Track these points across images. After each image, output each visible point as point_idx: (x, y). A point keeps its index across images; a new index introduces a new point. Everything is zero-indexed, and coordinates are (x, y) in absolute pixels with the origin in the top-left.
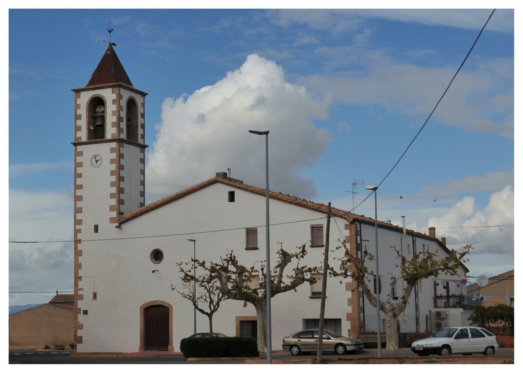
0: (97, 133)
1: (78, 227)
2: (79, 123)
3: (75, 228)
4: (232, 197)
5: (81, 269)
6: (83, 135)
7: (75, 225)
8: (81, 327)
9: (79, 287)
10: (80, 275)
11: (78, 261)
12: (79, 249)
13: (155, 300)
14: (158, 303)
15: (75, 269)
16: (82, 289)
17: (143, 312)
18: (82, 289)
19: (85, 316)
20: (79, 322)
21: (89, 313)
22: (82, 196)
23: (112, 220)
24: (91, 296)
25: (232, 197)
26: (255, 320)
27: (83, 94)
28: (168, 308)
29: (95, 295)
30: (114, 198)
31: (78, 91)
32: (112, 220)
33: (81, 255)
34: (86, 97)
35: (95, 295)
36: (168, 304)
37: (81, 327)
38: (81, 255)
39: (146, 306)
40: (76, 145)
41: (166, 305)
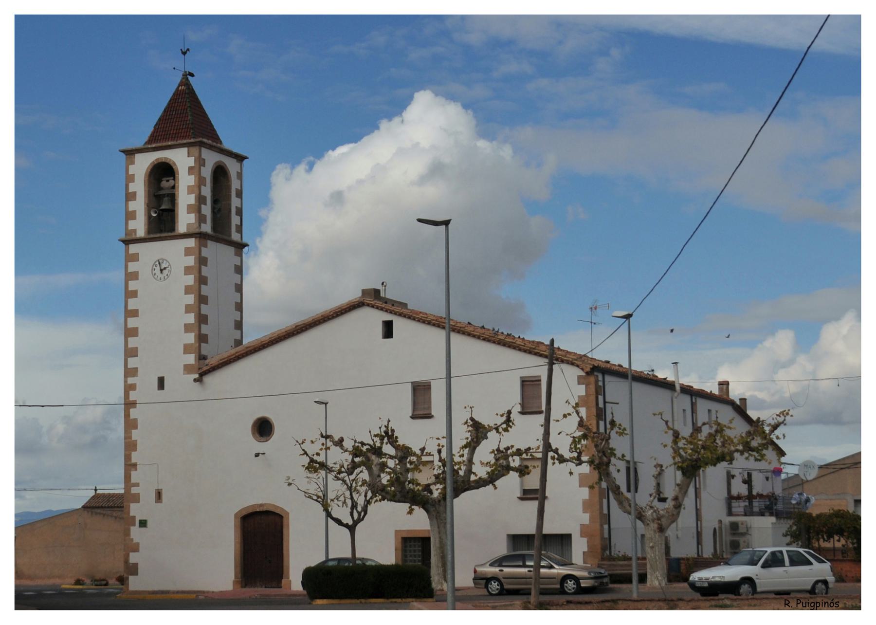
0: (162, 223)
1: (131, 380)
2: (132, 206)
3: (126, 382)
4: (388, 330)
6: (139, 226)
7: (126, 376)
8: (136, 548)
10: (133, 461)
11: (131, 438)
12: (132, 417)
14: (265, 509)
16: (137, 485)
17: (239, 524)
18: (137, 485)
19: (143, 529)
20: (132, 540)
21: (149, 524)
22: (137, 328)
23: (188, 369)
24: (153, 496)
25: (388, 330)
27: (138, 157)
28: (281, 517)
29: (159, 495)
30: (191, 331)
31: (130, 153)
32: (188, 369)
34: (144, 163)
35: (159, 495)
37: (136, 548)
39: (245, 513)
40: (127, 242)
41: (278, 511)
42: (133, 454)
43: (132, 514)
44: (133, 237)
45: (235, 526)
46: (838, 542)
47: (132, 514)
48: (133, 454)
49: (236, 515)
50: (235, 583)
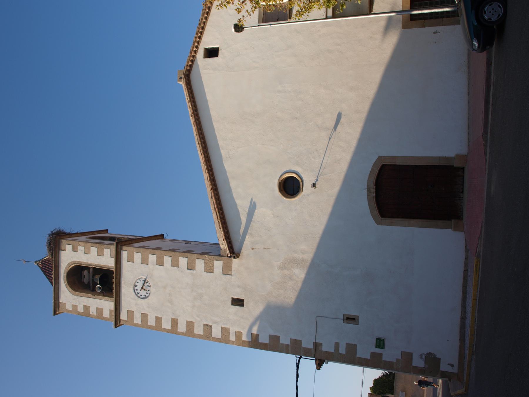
0: (103, 282)
1: (232, 338)
2: (93, 311)
3: (233, 343)
4: (212, 53)
5: (300, 341)
6: (106, 305)
7: (177, 333)
8: (408, 357)
9: (332, 350)
10: (311, 346)
11: (287, 346)
12: (267, 341)
13: (365, 192)
14: (373, 186)
15: (409, 372)
16: (337, 345)
17: (387, 220)
18: (337, 345)
19: (387, 343)
20: (397, 360)
21: (381, 336)
22: (187, 322)
23: (227, 271)
24: (349, 326)
25: (212, 53)
26: (413, 22)
27: (62, 300)
28: (383, 166)
29: (351, 319)
30: (194, 263)
31: (57, 307)
32: (227, 271)
33: (278, 338)
34: (68, 297)
35: (351, 319)
36: (375, 164)
37: (408, 357)
38: (278, 338)
39: (376, 212)
40: (117, 322)
41: (377, 170)
42: (304, 345)
43: (394, 361)
44: (114, 311)
45: (391, 224)
46: (241, 303)
47: (394, 361)
48: (304, 345)
49: (378, 223)
50: (456, 228)
